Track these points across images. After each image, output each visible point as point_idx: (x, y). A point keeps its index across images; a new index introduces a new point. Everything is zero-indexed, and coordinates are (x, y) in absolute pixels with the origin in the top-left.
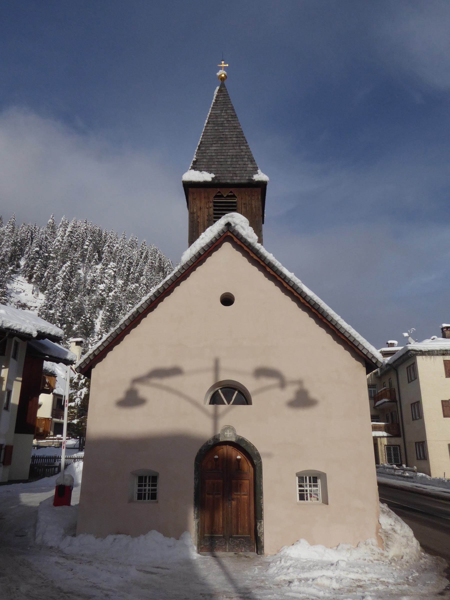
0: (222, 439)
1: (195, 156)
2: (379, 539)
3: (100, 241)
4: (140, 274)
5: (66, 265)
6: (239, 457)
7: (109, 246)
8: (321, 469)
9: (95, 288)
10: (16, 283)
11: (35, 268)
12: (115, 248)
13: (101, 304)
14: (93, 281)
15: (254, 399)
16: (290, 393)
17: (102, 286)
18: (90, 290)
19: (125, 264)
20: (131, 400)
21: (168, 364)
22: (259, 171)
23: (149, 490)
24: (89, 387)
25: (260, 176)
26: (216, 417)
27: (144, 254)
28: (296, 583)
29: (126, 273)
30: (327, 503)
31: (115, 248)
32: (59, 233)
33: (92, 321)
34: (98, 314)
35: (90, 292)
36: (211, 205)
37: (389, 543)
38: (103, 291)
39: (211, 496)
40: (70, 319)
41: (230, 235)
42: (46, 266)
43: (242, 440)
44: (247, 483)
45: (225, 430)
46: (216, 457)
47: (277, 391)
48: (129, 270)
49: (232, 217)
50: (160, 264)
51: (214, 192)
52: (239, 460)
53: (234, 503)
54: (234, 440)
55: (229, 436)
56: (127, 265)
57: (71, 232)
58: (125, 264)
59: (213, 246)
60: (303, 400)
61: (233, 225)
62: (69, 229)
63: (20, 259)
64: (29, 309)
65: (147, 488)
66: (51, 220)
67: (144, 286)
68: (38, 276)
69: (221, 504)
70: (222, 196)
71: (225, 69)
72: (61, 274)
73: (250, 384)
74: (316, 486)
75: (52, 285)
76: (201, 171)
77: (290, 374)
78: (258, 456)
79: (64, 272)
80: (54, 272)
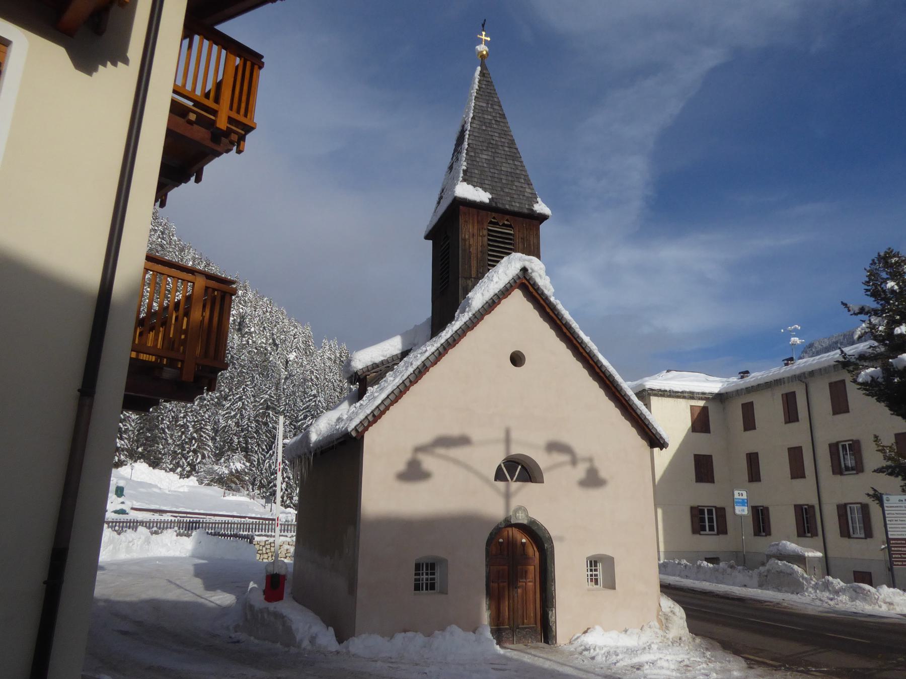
0: (513, 521)
1: (465, 163)
2: (660, 621)
6: (524, 540)
8: (609, 552)
15: (546, 477)
16: (580, 472)
20: (414, 472)
21: (455, 431)
22: (539, 199)
23: (427, 580)
25: (541, 207)
26: (508, 496)
28: (647, 667)
30: (613, 587)
36: (485, 232)
37: (670, 625)
39: (496, 585)
41: (524, 283)
43: (533, 522)
44: (533, 570)
45: (516, 511)
46: (501, 540)
47: (568, 468)
49: (530, 261)
51: (491, 217)
52: (523, 544)
53: (520, 591)
54: (525, 522)
55: (521, 519)
59: (505, 292)
60: (593, 480)
61: (530, 271)
65: (425, 577)
69: (507, 593)
70: (497, 224)
71: (487, 43)
73: (542, 460)
74: (596, 570)
76: (475, 186)
77: (581, 450)
78: (550, 540)
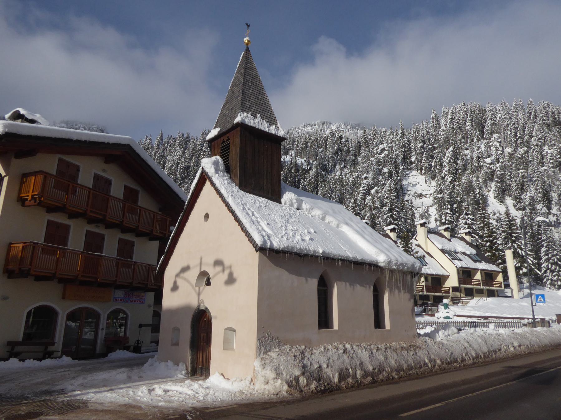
3: (482, 117)
4: (530, 136)
5: (449, 150)
7: (491, 119)
9: (482, 164)
10: (411, 178)
11: (423, 161)
12: (498, 119)
13: (490, 177)
14: (479, 158)
17: (488, 160)
18: (477, 167)
19: (511, 131)
24: (125, 326)
27: (533, 114)
29: (514, 140)
31: (498, 119)
32: (442, 122)
33: (483, 196)
34: (490, 187)
35: (479, 168)
38: (490, 164)
40: (459, 199)
42: (432, 157)
48: (516, 135)
50: (555, 119)
56: (513, 131)
57: (451, 119)
58: (511, 131)
62: (449, 117)
63: (411, 157)
64: (426, 197)
66: (433, 115)
67: (536, 147)
68: (426, 167)
72: (446, 160)
75: (440, 172)
79: (448, 157)
80: (440, 160)
